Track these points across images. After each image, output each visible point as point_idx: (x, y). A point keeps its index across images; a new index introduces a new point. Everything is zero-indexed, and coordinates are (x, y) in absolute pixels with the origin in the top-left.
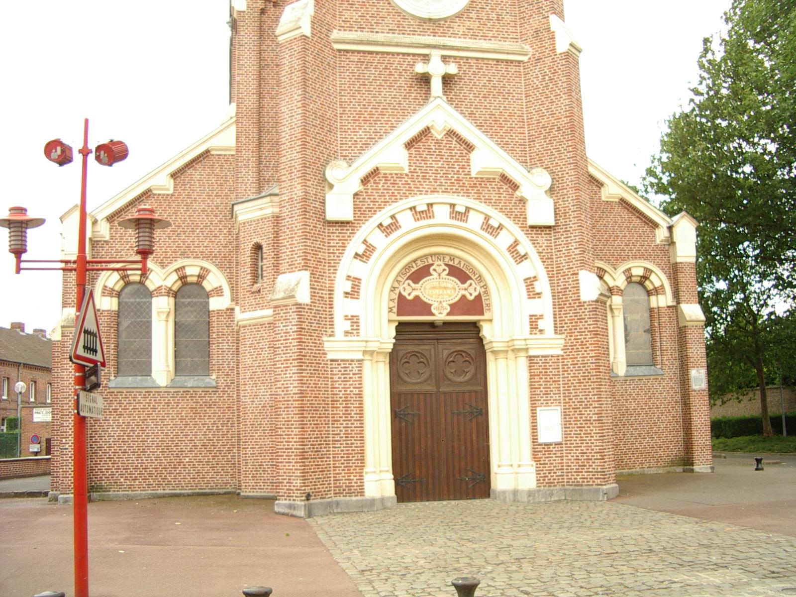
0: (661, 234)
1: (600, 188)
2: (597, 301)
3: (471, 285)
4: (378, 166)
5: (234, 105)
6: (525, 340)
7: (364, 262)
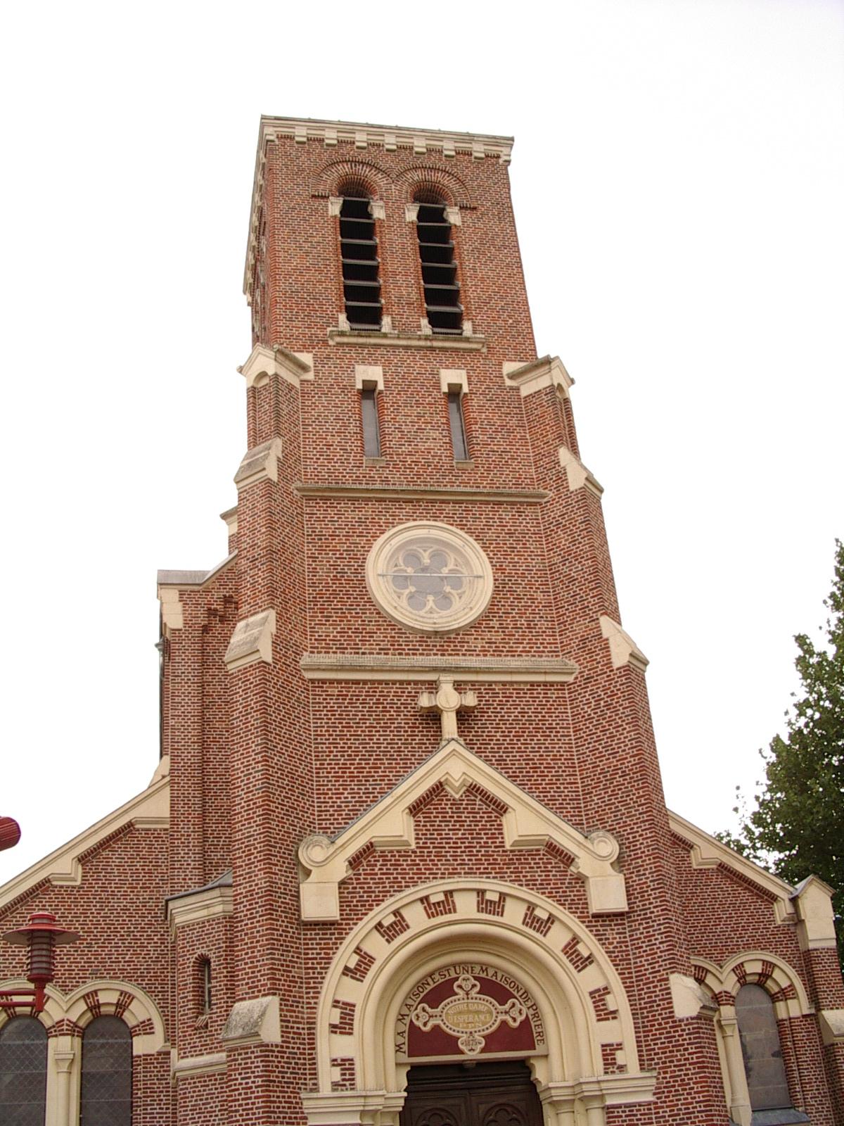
0: (782, 910)
1: (689, 852)
2: (698, 1017)
3: (514, 1005)
4: (373, 840)
5: (167, 759)
6: (598, 1082)
7: (358, 980)
